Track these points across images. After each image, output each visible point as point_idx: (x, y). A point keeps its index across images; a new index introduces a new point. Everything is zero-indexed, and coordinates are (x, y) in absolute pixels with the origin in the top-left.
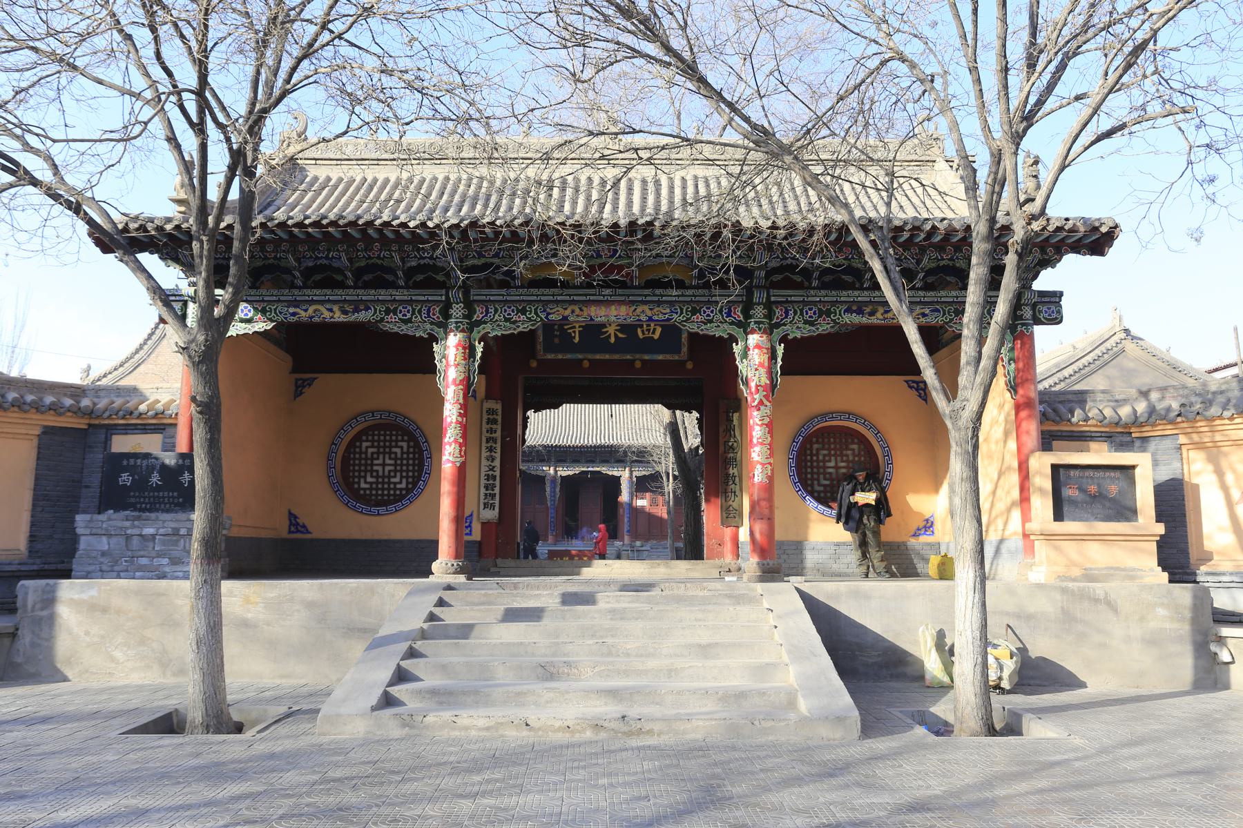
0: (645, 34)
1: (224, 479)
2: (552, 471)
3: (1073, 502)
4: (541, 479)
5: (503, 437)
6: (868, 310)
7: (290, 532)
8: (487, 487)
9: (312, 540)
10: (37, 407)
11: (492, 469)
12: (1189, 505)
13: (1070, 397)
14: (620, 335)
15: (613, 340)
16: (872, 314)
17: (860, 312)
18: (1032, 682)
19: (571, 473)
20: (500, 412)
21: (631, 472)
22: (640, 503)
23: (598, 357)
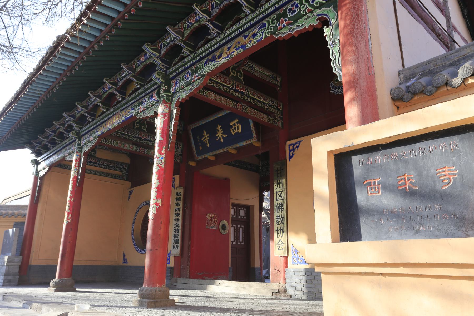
1: (452, 239)
5: (184, 207)
6: (218, 54)
7: (123, 263)
8: (175, 237)
9: (127, 266)
10: (13, 215)
11: (177, 226)
14: (225, 136)
15: (222, 140)
17: (213, 59)
20: (182, 194)
23: (218, 152)
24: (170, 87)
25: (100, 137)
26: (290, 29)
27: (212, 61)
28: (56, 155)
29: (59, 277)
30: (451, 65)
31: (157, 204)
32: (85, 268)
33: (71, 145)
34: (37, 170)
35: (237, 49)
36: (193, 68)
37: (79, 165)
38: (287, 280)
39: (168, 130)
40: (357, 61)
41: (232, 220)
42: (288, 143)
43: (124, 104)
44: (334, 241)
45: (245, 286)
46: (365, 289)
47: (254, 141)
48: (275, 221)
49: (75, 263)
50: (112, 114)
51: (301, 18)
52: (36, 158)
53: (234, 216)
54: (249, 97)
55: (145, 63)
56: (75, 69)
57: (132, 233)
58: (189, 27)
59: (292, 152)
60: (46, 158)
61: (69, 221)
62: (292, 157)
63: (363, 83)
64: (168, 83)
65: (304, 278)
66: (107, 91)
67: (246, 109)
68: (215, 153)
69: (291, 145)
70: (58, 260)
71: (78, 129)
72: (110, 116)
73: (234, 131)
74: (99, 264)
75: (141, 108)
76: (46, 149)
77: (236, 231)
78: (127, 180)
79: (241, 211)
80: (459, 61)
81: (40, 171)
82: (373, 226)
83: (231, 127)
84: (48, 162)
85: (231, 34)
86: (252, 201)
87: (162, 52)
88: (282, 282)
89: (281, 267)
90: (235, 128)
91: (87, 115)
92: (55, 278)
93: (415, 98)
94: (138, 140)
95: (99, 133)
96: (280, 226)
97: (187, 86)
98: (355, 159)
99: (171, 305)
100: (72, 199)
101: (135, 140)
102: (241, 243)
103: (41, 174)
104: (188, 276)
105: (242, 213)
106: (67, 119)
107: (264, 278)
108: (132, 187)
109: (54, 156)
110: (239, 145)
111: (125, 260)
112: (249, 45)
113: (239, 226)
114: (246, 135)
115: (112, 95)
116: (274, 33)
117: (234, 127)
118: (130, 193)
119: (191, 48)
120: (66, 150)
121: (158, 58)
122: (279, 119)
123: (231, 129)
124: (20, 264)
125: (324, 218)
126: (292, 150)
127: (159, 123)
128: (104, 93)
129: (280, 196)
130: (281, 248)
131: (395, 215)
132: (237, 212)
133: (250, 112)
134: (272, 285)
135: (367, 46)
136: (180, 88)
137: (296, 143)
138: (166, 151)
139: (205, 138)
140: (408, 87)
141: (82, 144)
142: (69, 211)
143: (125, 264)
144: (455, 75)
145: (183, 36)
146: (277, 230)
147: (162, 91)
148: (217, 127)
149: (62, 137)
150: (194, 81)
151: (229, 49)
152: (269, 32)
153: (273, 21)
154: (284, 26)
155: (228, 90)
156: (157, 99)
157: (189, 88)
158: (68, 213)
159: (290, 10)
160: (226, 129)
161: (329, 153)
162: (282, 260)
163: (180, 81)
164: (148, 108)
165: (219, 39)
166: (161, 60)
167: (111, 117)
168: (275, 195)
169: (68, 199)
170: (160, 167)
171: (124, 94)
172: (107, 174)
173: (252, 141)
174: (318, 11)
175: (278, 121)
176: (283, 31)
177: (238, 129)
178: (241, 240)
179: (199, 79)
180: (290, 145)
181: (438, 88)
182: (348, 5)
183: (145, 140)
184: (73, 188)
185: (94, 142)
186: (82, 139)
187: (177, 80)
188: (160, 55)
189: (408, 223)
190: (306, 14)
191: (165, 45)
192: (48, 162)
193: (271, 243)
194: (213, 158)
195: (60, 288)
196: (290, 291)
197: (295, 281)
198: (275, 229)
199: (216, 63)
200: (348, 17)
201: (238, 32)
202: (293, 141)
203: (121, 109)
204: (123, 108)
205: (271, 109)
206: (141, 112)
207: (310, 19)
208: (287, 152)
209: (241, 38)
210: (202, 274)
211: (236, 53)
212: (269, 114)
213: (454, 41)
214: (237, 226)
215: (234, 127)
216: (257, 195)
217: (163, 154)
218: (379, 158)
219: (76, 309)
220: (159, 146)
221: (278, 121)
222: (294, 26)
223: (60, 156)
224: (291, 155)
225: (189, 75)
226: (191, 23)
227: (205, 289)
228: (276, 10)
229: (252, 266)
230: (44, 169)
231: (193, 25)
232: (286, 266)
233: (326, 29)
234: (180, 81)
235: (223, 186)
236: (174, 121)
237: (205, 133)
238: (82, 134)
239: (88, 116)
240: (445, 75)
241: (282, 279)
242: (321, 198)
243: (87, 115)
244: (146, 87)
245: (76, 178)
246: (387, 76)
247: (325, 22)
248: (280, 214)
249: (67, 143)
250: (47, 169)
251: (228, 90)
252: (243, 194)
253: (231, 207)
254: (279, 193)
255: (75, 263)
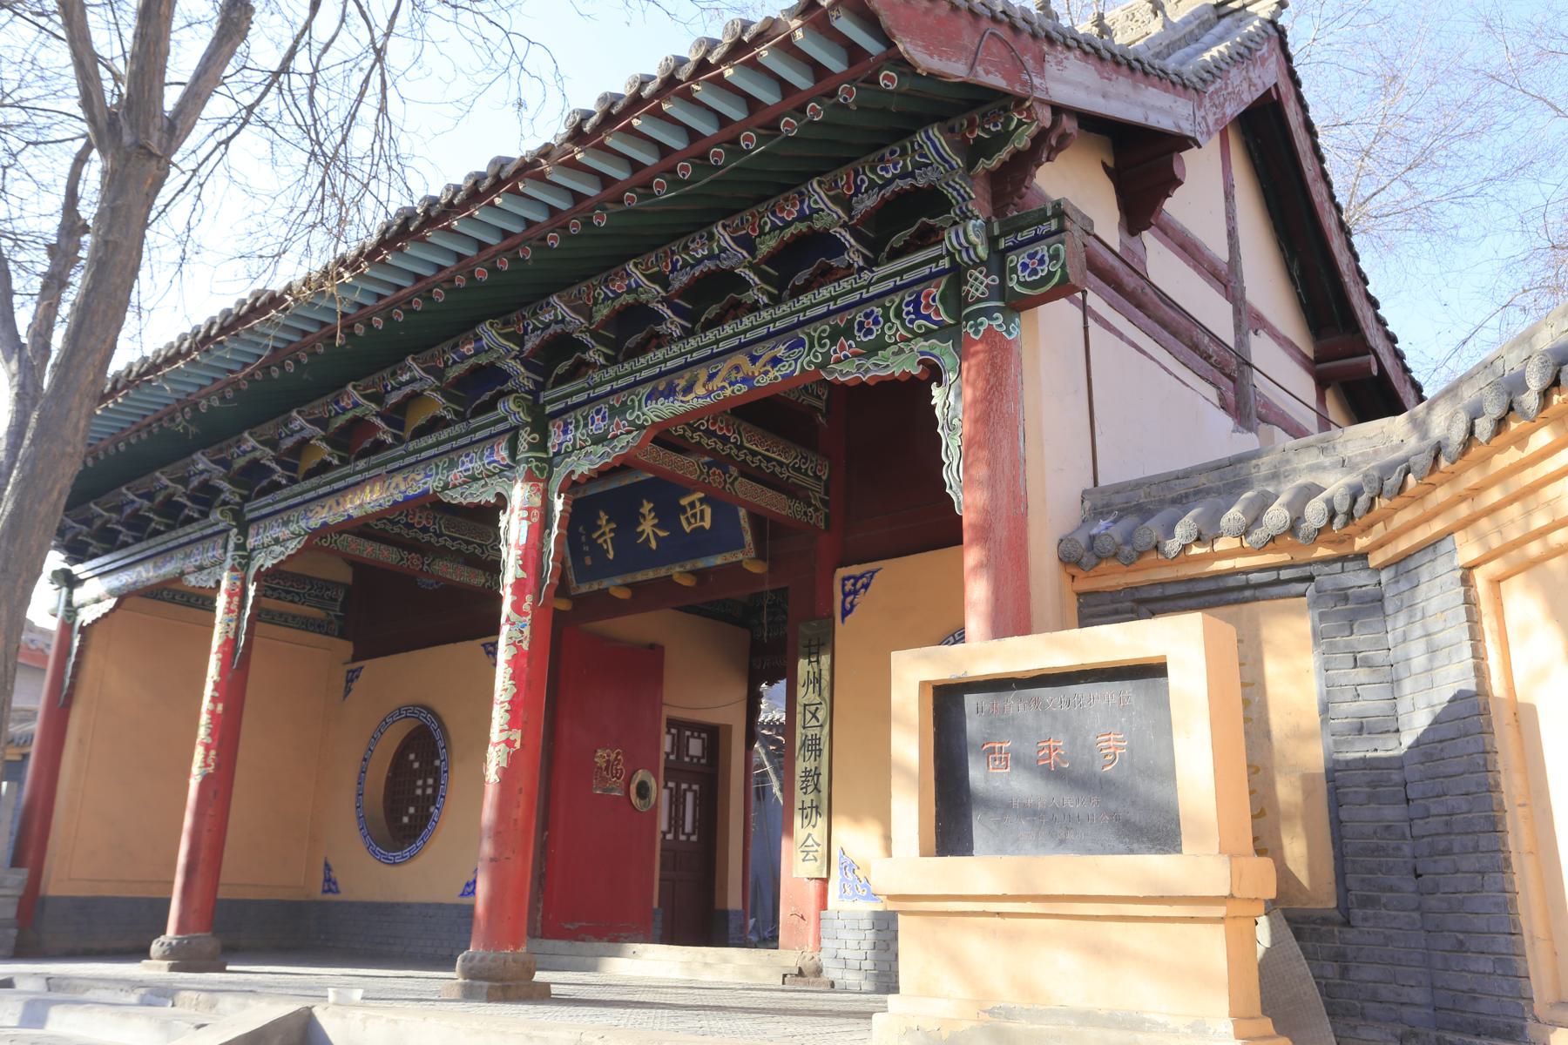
3: (1003, 807)
6: (682, 383)
9: (338, 903)
12: (1511, 786)
13: (1202, 481)
14: (662, 534)
15: (653, 545)
16: (688, 389)
17: (670, 392)
23: (640, 577)
24: (545, 436)
25: (314, 533)
26: (859, 367)
27: (667, 398)
28: (150, 565)
29: (181, 928)
30: (1174, 502)
31: (509, 743)
32: (232, 903)
33: (208, 543)
34: (69, 603)
35: (731, 384)
36: (613, 401)
37: (242, 606)
38: (825, 943)
39: (540, 554)
40: (992, 483)
41: (666, 769)
42: (842, 572)
43: (402, 457)
44: (923, 854)
45: (710, 960)
46: (975, 944)
47: (744, 556)
48: (798, 784)
49: (220, 896)
50: (359, 478)
51: (884, 349)
52: (66, 566)
53: (672, 757)
54: (740, 447)
55: (472, 361)
56: (282, 368)
57: (358, 801)
58: (607, 298)
59: (849, 599)
60: (107, 568)
61: (211, 770)
62: (850, 611)
63: (1001, 532)
64: (541, 425)
65: (870, 935)
66: (345, 410)
67: (732, 484)
68: (629, 579)
69: (848, 578)
70: (172, 883)
71: (238, 499)
72: (351, 480)
73: (689, 523)
74: (251, 895)
75: (456, 475)
76: (108, 541)
77: (676, 801)
78: (342, 635)
79: (692, 741)
80: (1187, 496)
81: (83, 606)
82: (994, 827)
83: (683, 510)
84: (115, 581)
85: (717, 342)
86: (725, 709)
87: (529, 346)
88: (809, 949)
89: (811, 908)
90: (694, 515)
91: (274, 465)
92: (164, 932)
93: (1103, 565)
94: (404, 532)
95: (315, 523)
96: (812, 796)
97: (595, 443)
98: (971, 701)
99: (542, 995)
100: (220, 707)
101: (396, 530)
102: (689, 835)
103: (86, 616)
104: (539, 932)
105: (695, 747)
106: (201, 467)
107: (767, 937)
108: (355, 659)
109: (140, 568)
110: (702, 563)
111: (330, 884)
112: (763, 381)
113: (684, 786)
114: (724, 536)
115: (359, 425)
116: (823, 366)
117: (689, 513)
118: (352, 677)
119: (606, 346)
120: (187, 556)
121: (515, 358)
122: (819, 505)
123: (682, 518)
124: (19, 892)
125: (909, 809)
126: (850, 593)
127: (514, 529)
128: (337, 414)
129: (814, 716)
130: (810, 856)
131: (1031, 813)
132: (680, 745)
133: (745, 489)
134: (787, 957)
135: (1014, 448)
136: (574, 445)
137: (862, 576)
138: (533, 607)
139: (603, 534)
140: (1092, 538)
141: (249, 546)
142: (209, 740)
143: (330, 897)
144: (1170, 533)
145: (590, 318)
146: (803, 809)
147: (523, 445)
148: (642, 505)
149: (173, 514)
150: (615, 437)
151: (711, 377)
152: (810, 362)
153: (820, 338)
154: (846, 357)
155: (689, 433)
156: (508, 461)
157: (600, 449)
158: (207, 748)
159: (861, 324)
160: (669, 514)
161: (923, 684)
162: (813, 888)
163: (576, 428)
164: (474, 479)
165: (688, 348)
166: (525, 363)
167: (357, 484)
168: (799, 709)
169: (206, 704)
170: (519, 648)
171: (400, 425)
172: (281, 615)
173: (740, 556)
174: (921, 344)
175: (817, 510)
176: (845, 367)
177: (702, 519)
178: (688, 828)
179: (629, 432)
180: (845, 579)
181: (1141, 554)
182: (981, 356)
183: (425, 530)
184: (222, 673)
185: (293, 546)
186: (252, 531)
187: (566, 424)
188: (521, 352)
189: (1052, 827)
190: (896, 343)
191: (535, 329)
192: (115, 581)
193: (785, 843)
194: (623, 594)
195: (184, 960)
196: (832, 972)
197: (845, 948)
198: (798, 805)
199: (677, 404)
200: (980, 384)
201: (735, 342)
202: (855, 570)
203: (391, 466)
204: (396, 465)
205: (797, 479)
206: (455, 486)
207: (903, 357)
208: (838, 597)
209: (741, 359)
210: (577, 925)
211: (728, 392)
212: (791, 491)
213: (1250, 365)
214: (678, 786)
215: (689, 513)
216: (741, 692)
217: (526, 614)
218: (1012, 702)
219: (332, 998)
220: (513, 593)
221: (817, 510)
222: (869, 363)
223: (169, 568)
224: (848, 606)
225: (603, 419)
226: (613, 292)
227: (593, 968)
228: (829, 313)
229: (718, 906)
230: (98, 601)
231: (618, 296)
232: (823, 905)
233: (936, 392)
234: (576, 428)
235: (647, 664)
236: (555, 531)
237: (604, 518)
238: (250, 516)
239: (278, 468)
240: (1154, 527)
241: (811, 940)
242: (905, 771)
243: (274, 465)
244: (475, 422)
245: (230, 644)
246: (1054, 504)
247: (934, 373)
248: (811, 765)
249: (193, 536)
250: (110, 603)
251: (689, 433)
252: (701, 692)
253: (664, 728)
254: (813, 708)
255: (220, 896)
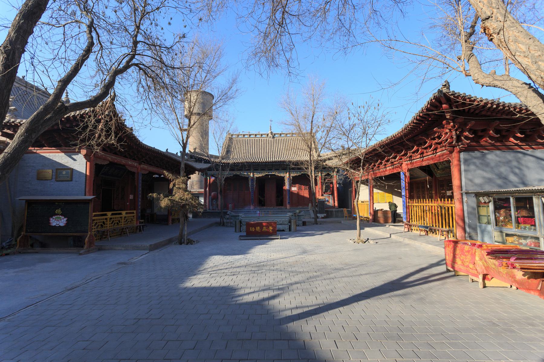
0: (493, 145)
2: (252, 175)
4: (246, 179)
18: (536, 256)
19: (260, 175)
21: (290, 175)
22: (294, 189)
